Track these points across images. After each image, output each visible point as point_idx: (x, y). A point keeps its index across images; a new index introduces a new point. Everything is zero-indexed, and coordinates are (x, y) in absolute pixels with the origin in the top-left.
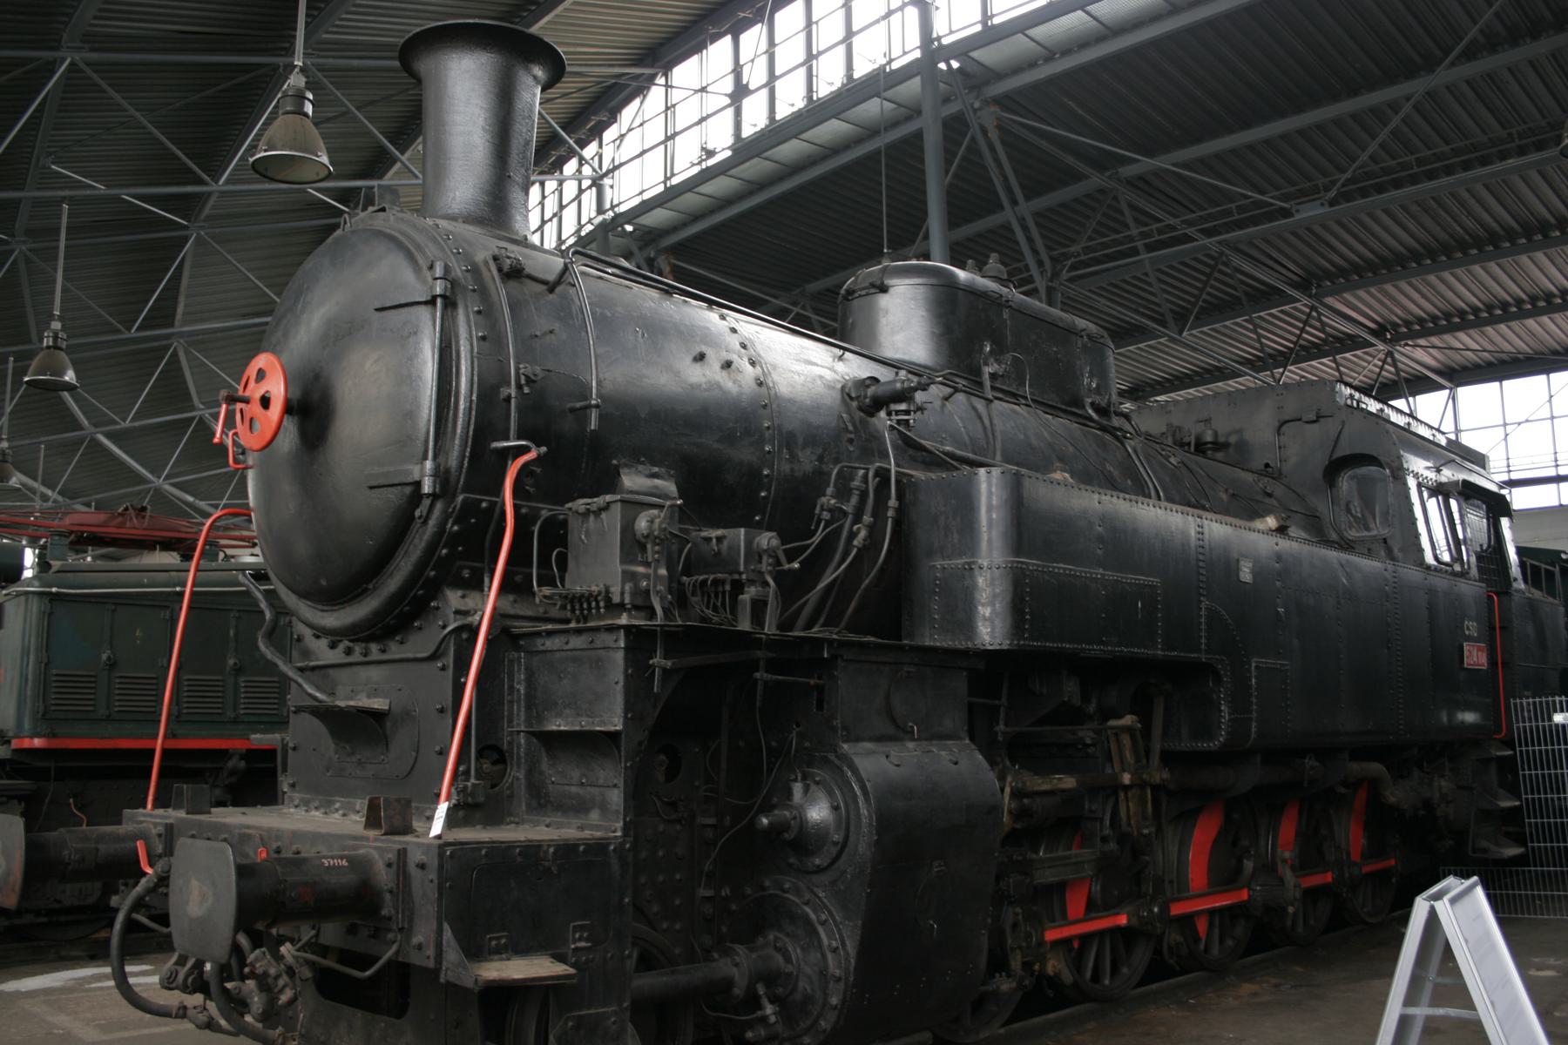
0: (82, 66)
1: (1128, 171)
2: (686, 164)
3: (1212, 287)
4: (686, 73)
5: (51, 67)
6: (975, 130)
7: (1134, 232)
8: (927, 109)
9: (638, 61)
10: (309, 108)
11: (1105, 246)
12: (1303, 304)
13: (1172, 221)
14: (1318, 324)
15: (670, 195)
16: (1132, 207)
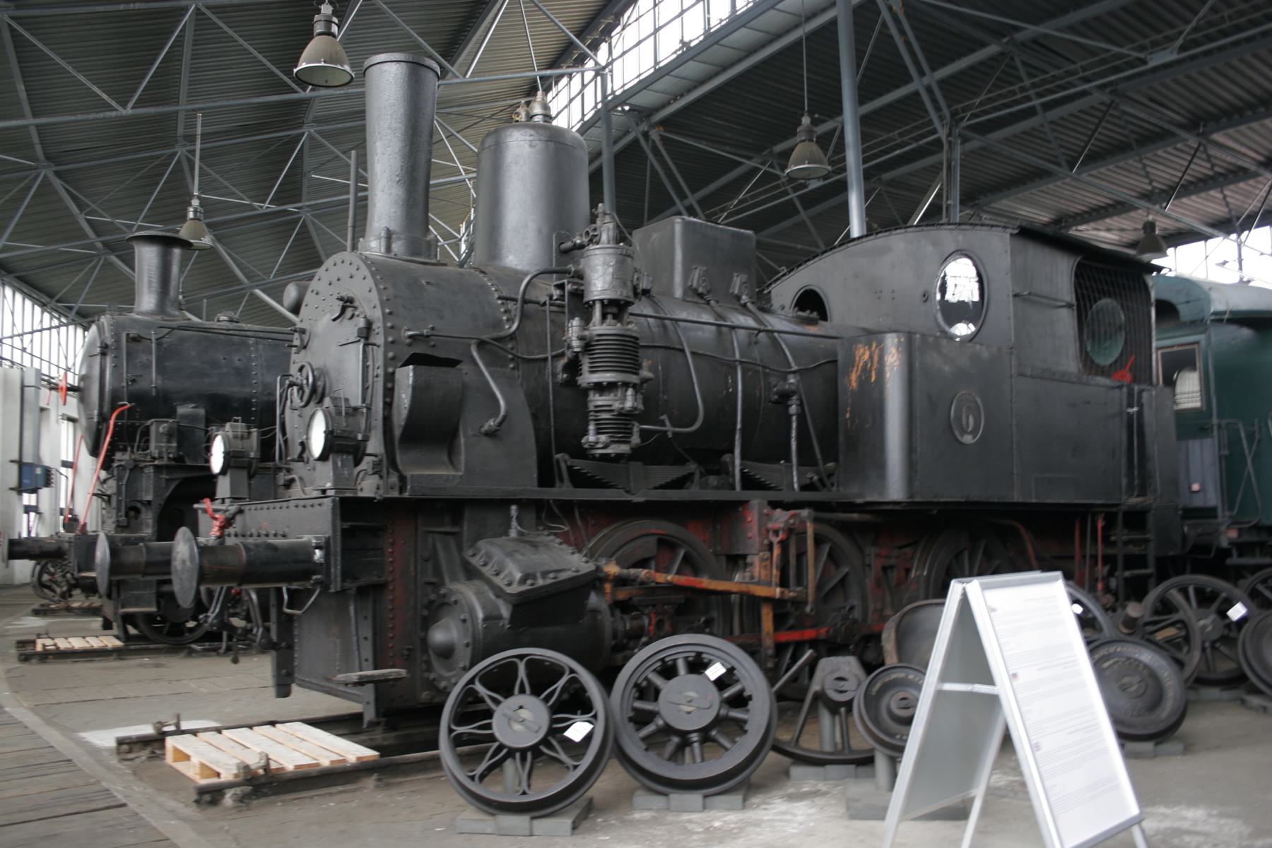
1: (1019, 36)
2: (668, 50)
3: (1104, 128)
7: (1027, 83)
11: (1001, 96)
12: (1193, 142)
13: (752, 164)
14: (1204, 156)
15: (660, 73)
16: (1025, 64)
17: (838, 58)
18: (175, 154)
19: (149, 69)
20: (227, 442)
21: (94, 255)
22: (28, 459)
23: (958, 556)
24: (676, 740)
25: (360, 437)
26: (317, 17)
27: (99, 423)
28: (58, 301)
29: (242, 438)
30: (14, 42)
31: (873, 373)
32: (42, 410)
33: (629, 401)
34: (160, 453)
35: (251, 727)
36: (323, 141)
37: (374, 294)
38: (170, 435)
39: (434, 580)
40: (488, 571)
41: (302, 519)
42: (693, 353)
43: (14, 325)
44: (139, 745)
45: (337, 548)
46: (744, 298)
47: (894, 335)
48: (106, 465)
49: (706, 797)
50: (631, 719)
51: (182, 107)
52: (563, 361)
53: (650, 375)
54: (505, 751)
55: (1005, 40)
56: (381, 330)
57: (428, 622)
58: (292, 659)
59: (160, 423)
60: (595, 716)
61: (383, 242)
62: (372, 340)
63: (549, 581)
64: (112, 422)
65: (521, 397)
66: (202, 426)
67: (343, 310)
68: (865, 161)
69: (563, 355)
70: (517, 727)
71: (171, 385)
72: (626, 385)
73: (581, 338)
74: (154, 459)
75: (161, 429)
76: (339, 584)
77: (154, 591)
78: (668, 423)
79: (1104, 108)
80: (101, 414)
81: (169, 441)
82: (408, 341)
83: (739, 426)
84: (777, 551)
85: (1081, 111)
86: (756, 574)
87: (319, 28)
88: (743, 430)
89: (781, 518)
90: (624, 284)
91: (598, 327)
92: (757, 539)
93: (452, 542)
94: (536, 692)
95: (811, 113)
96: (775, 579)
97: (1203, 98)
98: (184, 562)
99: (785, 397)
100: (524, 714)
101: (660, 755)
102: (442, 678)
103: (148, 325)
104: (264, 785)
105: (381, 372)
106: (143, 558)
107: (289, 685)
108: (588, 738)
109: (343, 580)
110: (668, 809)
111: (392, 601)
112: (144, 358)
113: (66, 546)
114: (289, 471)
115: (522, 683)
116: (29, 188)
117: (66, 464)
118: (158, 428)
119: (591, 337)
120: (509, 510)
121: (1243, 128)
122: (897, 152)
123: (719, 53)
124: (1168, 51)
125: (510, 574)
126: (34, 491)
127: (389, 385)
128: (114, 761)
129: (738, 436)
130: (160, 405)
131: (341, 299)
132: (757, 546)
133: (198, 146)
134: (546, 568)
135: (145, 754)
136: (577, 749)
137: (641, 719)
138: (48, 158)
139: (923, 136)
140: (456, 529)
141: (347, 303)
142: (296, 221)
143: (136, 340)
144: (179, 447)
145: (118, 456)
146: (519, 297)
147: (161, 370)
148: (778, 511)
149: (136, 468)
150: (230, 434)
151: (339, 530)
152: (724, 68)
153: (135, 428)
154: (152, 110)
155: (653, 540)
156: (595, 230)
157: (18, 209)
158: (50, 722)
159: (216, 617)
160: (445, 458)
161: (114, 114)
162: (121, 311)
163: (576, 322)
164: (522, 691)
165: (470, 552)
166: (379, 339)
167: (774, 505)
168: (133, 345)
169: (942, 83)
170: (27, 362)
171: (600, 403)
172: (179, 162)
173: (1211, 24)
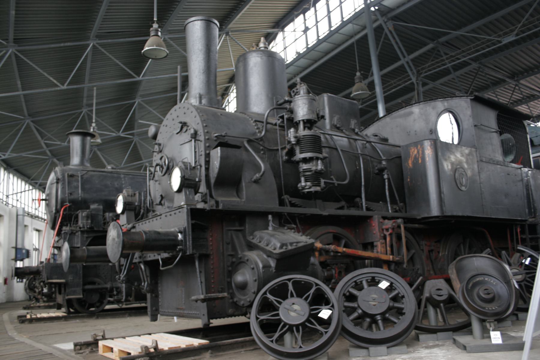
0: (98, 46)
3: (477, 81)
4: (289, 28)
5: (88, 45)
6: (386, 31)
8: (368, 26)
9: (274, 27)
10: (159, 34)
12: (512, 83)
14: (519, 92)
17: (368, 48)
18: (82, 112)
19: (75, 67)
20: (124, 198)
21: (46, 159)
22: (19, 246)
23: (459, 246)
24: (368, 320)
25: (197, 180)
26: (151, 29)
27: (55, 213)
28: (32, 180)
29: (132, 196)
30: (16, 60)
31: (420, 159)
32: (26, 226)
33: (320, 166)
34: (83, 225)
35: (140, 336)
36: (145, 105)
37: (198, 117)
38: (87, 217)
39: (232, 253)
40: (262, 245)
41: (171, 222)
42: (342, 150)
43: (13, 190)
44: (85, 346)
45: (189, 232)
46: (357, 130)
47: (428, 141)
48: (59, 234)
49: (388, 348)
50: (344, 311)
51: (86, 85)
52: (285, 151)
53: (327, 155)
54: (287, 327)
55: (435, 42)
56: (202, 134)
57: (231, 273)
58: (158, 302)
59: (83, 212)
60: (333, 306)
61: (198, 99)
62: (197, 138)
63: (293, 247)
64: (61, 213)
65: (268, 166)
66: (101, 213)
67: (182, 128)
68: (384, 92)
69: (285, 148)
70: (293, 314)
71: (87, 196)
72: (317, 159)
73: (295, 137)
74: (80, 228)
75: (84, 215)
76: (191, 250)
77: (84, 285)
78: (334, 179)
79: (476, 71)
80: (56, 209)
81: (87, 220)
82: (215, 138)
83: (363, 184)
84: (388, 239)
85: (466, 73)
86: (379, 250)
87: (152, 34)
88: (365, 186)
89: (388, 224)
90: (313, 112)
91: (303, 132)
92: (378, 234)
93: (240, 235)
94: (300, 296)
95: (360, 71)
96: (389, 252)
97: (516, 64)
98: (114, 239)
99: (381, 170)
100: (296, 307)
101: (361, 327)
102: (241, 300)
103: (77, 170)
104: (155, 356)
105: (203, 153)
106: (86, 254)
107: (157, 315)
108: (330, 318)
109: (193, 250)
110: (369, 356)
111: (213, 264)
112: (75, 184)
113: (41, 268)
114: (154, 211)
115: (291, 292)
116: (20, 129)
117: (36, 249)
118: (82, 214)
119: (300, 137)
120: (268, 217)
121: (533, 77)
122: (394, 90)
123: (314, 55)
124: (511, 36)
125: (274, 244)
126: (22, 260)
127: (207, 159)
128: (73, 354)
129: (363, 189)
130: (83, 204)
131: (181, 123)
132: (379, 237)
133: (94, 108)
134: (292, 241)
135: (88, 351)
136: (326, 323)
137: (349, 311)
138: (29, 115)
139: (406, 82)
140: (242, 228)
141: (184, 125)
142: (132, 142)
143: (71, 176)
144: (92, 223)
145: (64, 228)
146: (264, 121)
147: (83, 189)
148: (386, 221)
149: (72, 233)
150: (126, 194)
151: (190, 223)
152: (316, 61)
153: (72, 215)
154: (75, 87)
155: (331, 235)
156: (297, 89)
157: (15, 139)
158: (38, 342)
159: (125, 276)
160: (235, 194)
161: (59, 88)
162: (64, 165)
163: (292, 130)
164: (292, 296)
165: (251, 237)
166: (202, 138)
167: (384, 218)
168: (71, 179)
169: (412, 60)
170: (19, 206)
171: (305, 168)
172: (84, 116)
173: (530, 23)
